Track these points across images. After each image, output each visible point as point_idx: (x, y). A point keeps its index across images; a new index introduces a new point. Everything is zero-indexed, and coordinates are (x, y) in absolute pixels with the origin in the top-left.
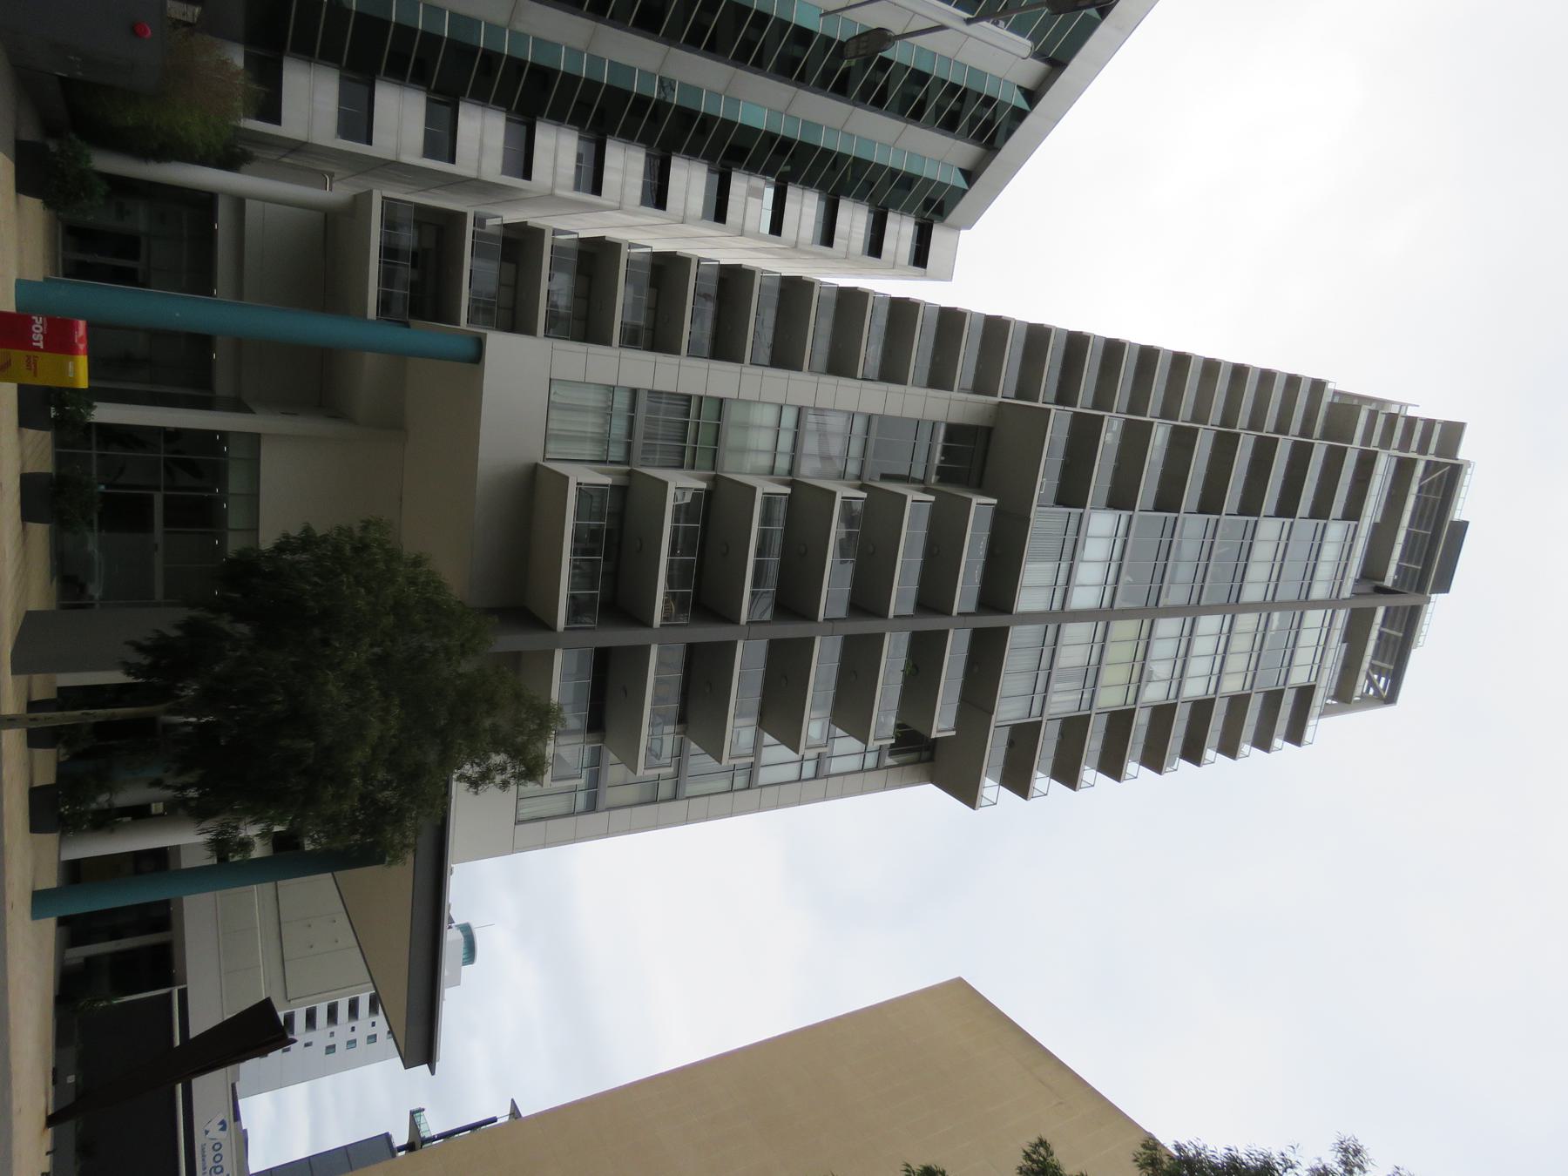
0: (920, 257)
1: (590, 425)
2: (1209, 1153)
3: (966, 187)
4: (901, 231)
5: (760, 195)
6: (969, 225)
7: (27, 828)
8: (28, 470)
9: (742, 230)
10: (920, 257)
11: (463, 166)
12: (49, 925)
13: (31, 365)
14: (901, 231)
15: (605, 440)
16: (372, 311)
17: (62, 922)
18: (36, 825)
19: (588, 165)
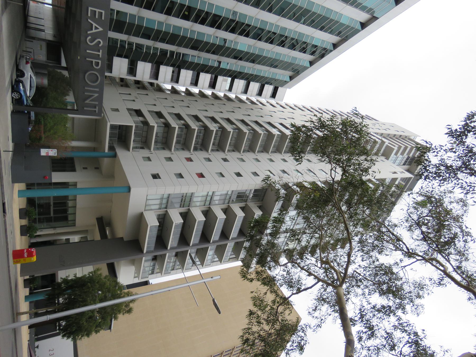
0: (274, 95)
1: (158, 202)
2: (401, 202)
3: (289, 81)
4: (268, 89)
5: (226, 81)
6: (290, 88)
7: (23, 287)
8: (21, 208)
9: (220, 90)
10: (274, 95)
11: (139, 77)
12: (28, 303)
13: (25, 260)
14: (268, 89)
15: (161, 204)
16: (106, 150)
17: (30, 303)
18: (22, 234)
19: (176, 75)
